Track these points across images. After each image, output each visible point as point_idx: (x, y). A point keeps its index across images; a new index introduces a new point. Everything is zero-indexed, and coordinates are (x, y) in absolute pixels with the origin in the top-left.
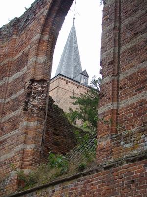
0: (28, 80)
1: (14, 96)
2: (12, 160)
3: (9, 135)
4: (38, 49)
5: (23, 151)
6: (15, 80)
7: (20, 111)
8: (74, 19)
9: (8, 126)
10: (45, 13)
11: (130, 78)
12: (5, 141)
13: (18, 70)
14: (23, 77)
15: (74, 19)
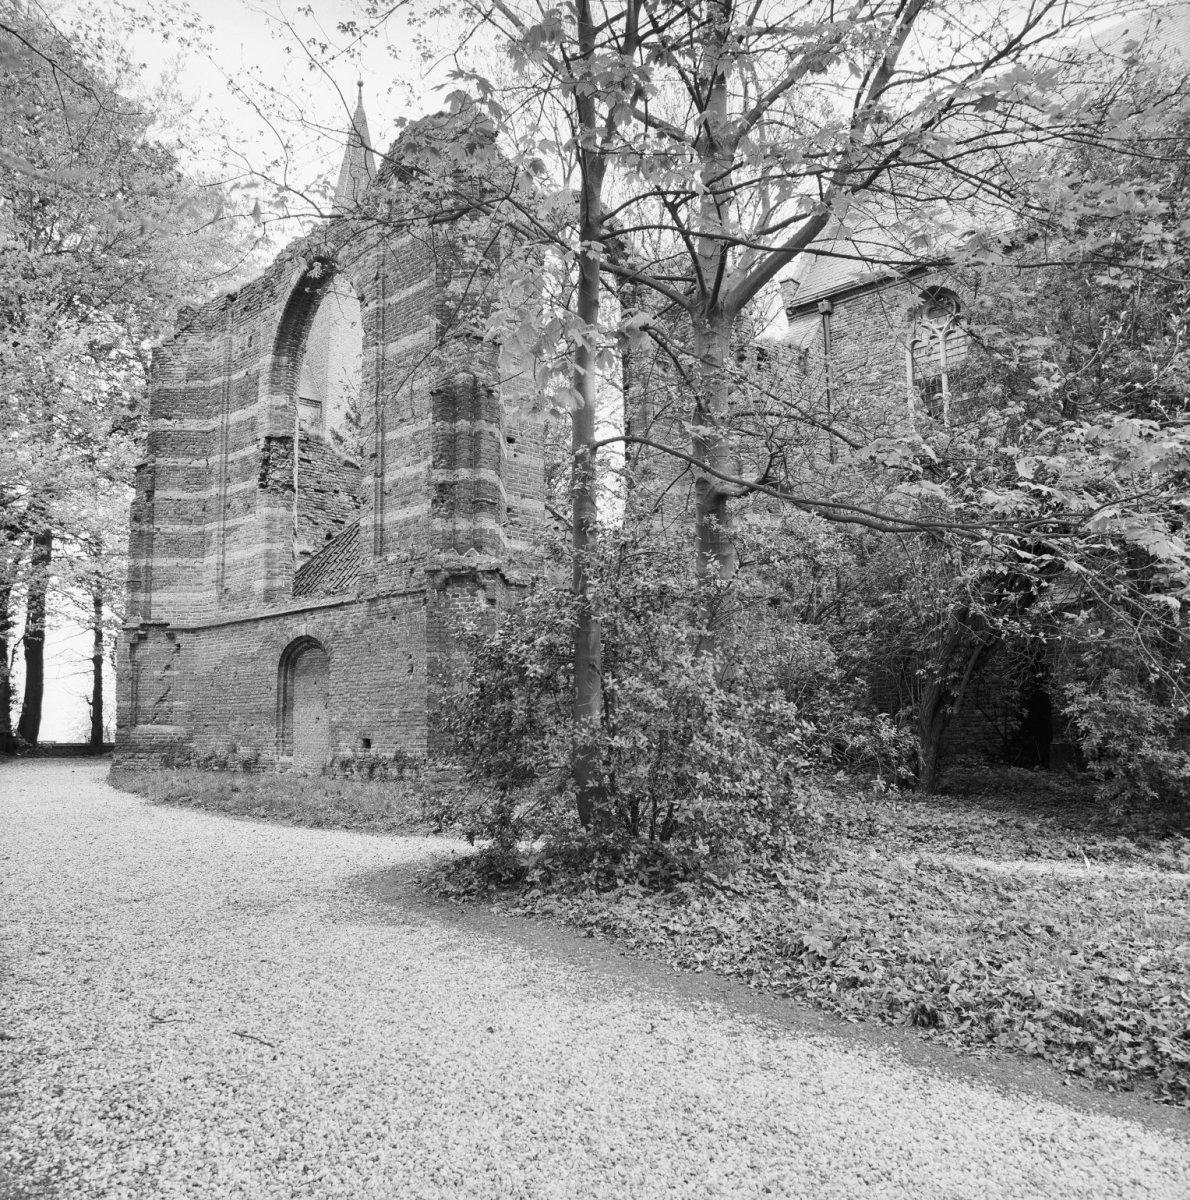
0: (262, 435)
1: (241, 453)
2: (251, 562)
3: (240, 521)
4: (273, 382)
5: (268, 554)
6: (239, 424)
7: (254, 482)
8: (360, 84)
9: (238, 504)
10: (279, 315)
11: (395, 485)
12: (235, 528)
13: (242, 406)
14: (252, 424)
15: (360, 84)
